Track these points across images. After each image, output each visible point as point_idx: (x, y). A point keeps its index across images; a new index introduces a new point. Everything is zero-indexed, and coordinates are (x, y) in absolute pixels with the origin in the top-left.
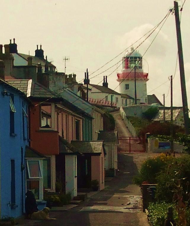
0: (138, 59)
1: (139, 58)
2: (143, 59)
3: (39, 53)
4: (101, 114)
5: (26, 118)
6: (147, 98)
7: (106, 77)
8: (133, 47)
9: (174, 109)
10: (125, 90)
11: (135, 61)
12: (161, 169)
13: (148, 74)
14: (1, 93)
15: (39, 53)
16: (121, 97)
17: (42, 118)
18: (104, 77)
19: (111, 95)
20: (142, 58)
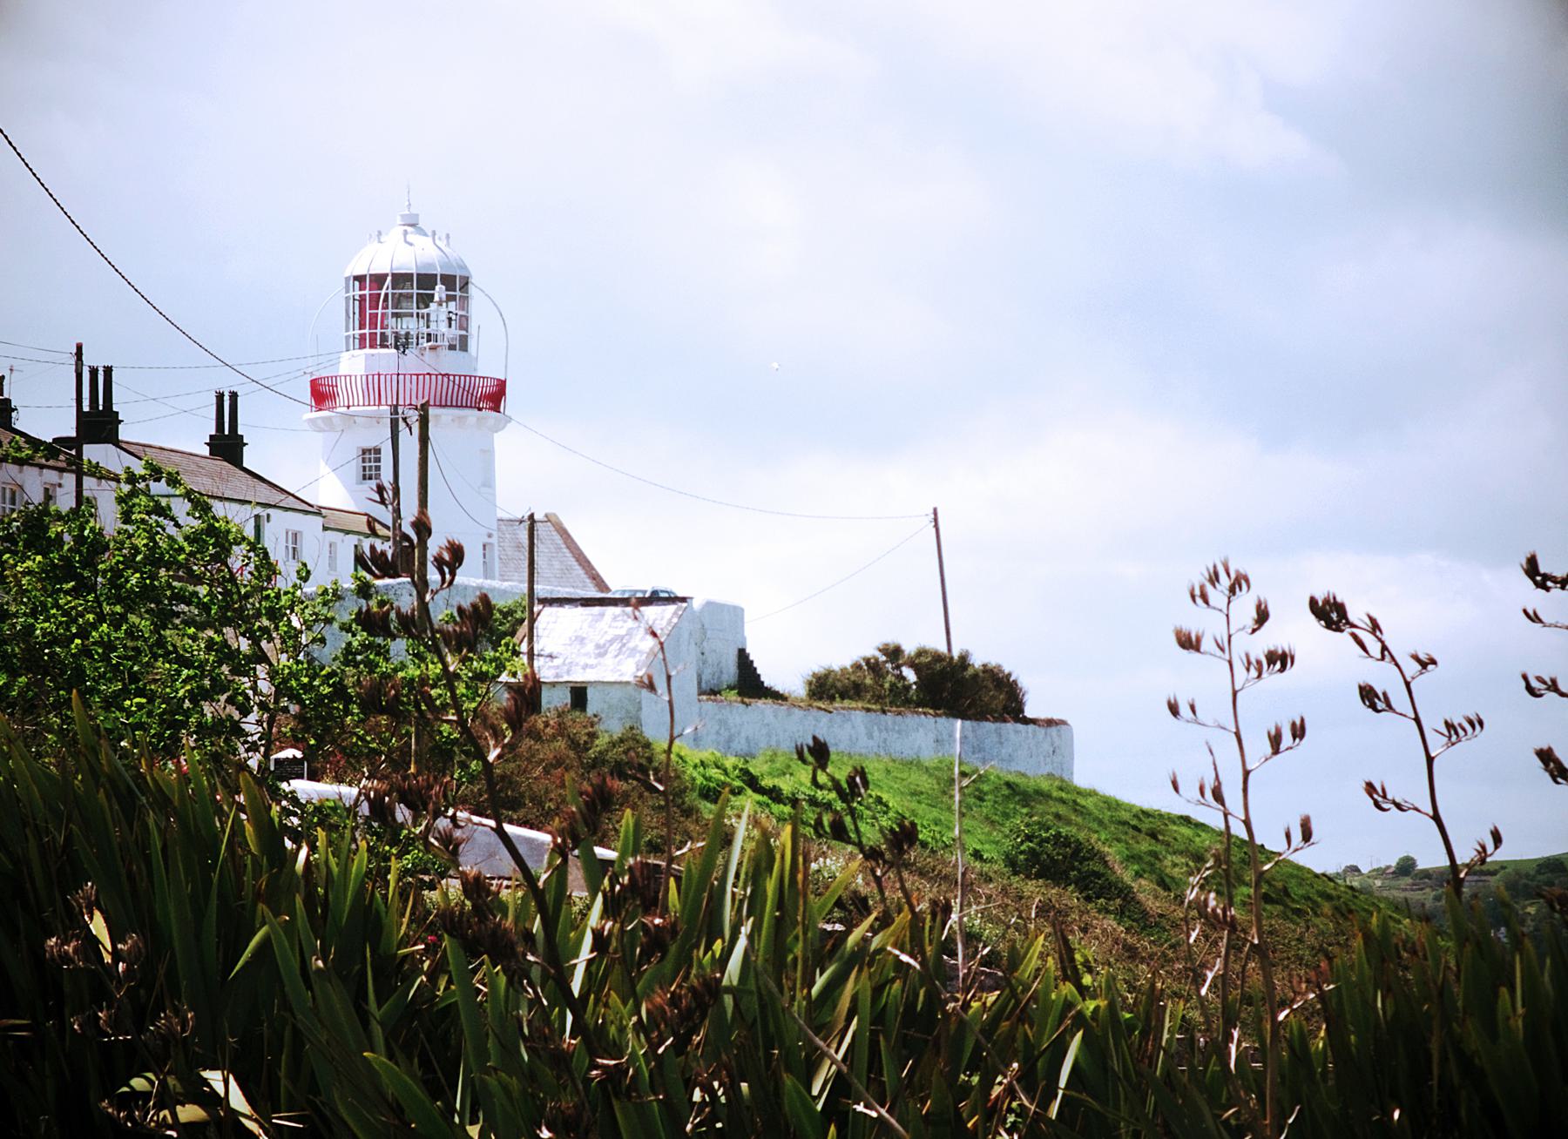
0: (439, 291)
1: (449, 281)
2: (472, 289)
3: (815, 738)
4: (1027, 721)
5: (588, 670)
6: (494, 540)
7: (234, 396)
8: (414, 211)
9: (757, 783)
10: (358, 483)
11: (426, 300)
12: (624, 865)
13: (502, 385)
14: (1069, 722)
15: (815, 738)
16: (325, 529)
17: (401, 674)
18: (220, 397)
19: (257, 517)
20: (465, 283)
